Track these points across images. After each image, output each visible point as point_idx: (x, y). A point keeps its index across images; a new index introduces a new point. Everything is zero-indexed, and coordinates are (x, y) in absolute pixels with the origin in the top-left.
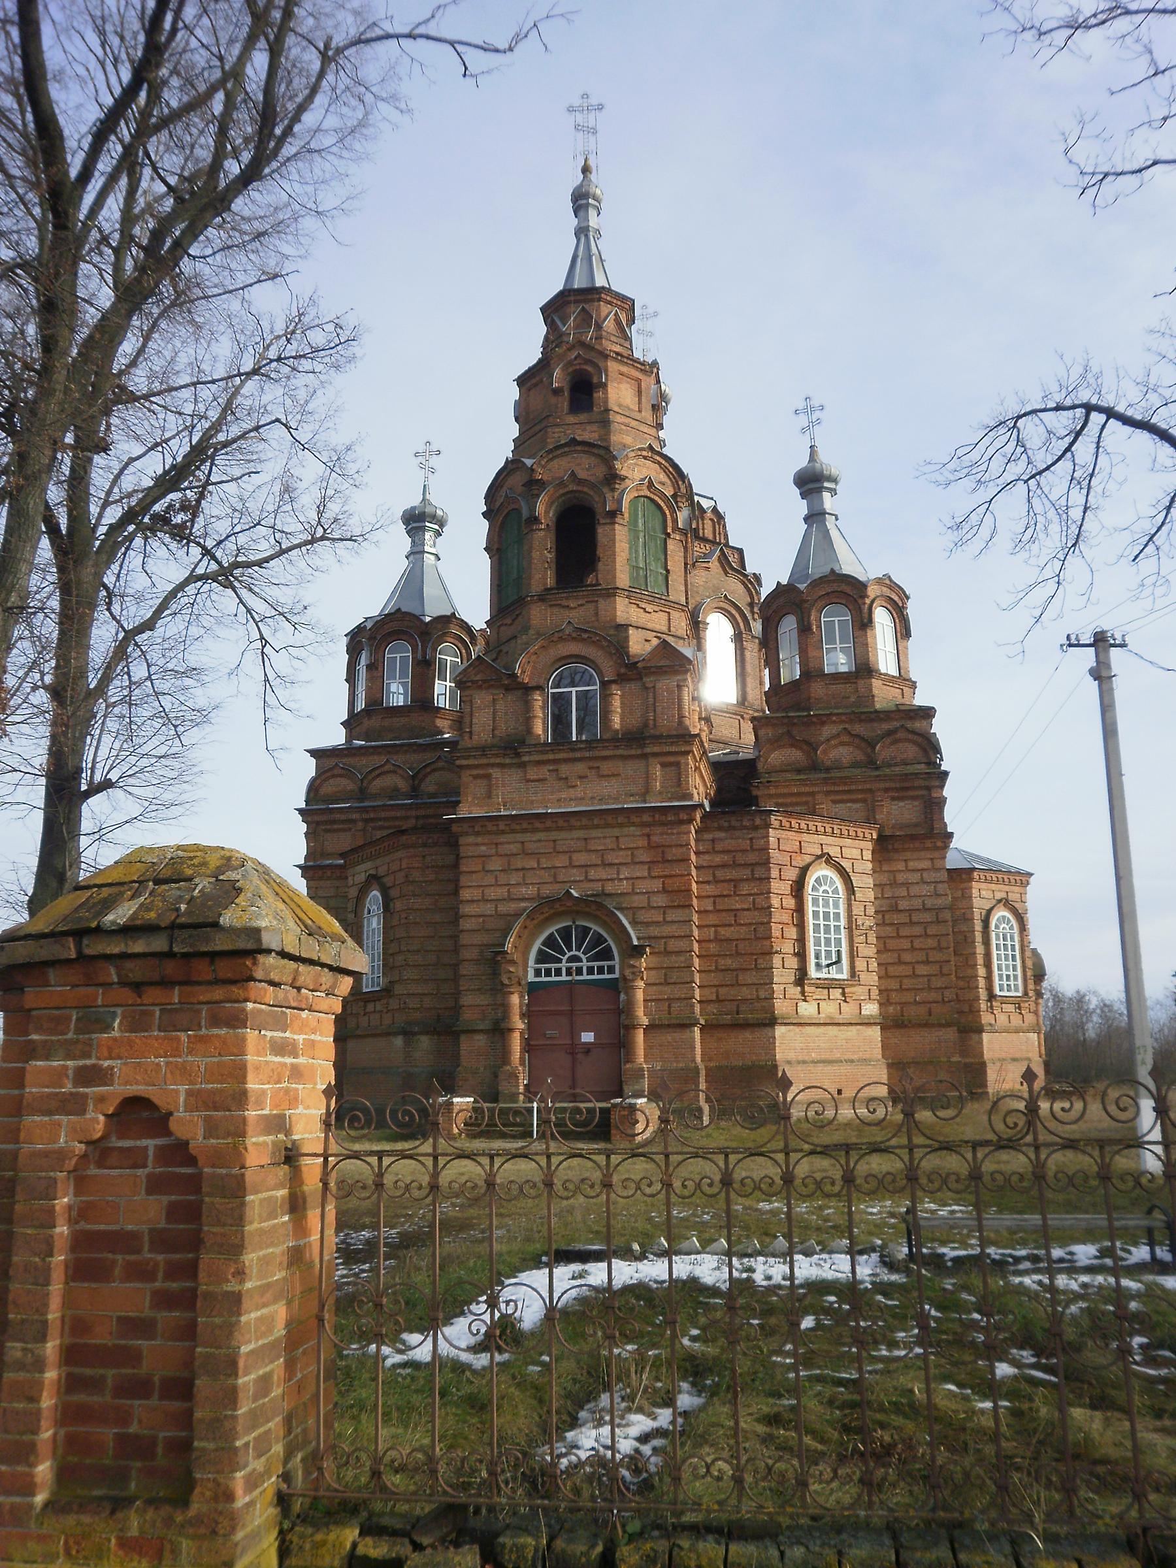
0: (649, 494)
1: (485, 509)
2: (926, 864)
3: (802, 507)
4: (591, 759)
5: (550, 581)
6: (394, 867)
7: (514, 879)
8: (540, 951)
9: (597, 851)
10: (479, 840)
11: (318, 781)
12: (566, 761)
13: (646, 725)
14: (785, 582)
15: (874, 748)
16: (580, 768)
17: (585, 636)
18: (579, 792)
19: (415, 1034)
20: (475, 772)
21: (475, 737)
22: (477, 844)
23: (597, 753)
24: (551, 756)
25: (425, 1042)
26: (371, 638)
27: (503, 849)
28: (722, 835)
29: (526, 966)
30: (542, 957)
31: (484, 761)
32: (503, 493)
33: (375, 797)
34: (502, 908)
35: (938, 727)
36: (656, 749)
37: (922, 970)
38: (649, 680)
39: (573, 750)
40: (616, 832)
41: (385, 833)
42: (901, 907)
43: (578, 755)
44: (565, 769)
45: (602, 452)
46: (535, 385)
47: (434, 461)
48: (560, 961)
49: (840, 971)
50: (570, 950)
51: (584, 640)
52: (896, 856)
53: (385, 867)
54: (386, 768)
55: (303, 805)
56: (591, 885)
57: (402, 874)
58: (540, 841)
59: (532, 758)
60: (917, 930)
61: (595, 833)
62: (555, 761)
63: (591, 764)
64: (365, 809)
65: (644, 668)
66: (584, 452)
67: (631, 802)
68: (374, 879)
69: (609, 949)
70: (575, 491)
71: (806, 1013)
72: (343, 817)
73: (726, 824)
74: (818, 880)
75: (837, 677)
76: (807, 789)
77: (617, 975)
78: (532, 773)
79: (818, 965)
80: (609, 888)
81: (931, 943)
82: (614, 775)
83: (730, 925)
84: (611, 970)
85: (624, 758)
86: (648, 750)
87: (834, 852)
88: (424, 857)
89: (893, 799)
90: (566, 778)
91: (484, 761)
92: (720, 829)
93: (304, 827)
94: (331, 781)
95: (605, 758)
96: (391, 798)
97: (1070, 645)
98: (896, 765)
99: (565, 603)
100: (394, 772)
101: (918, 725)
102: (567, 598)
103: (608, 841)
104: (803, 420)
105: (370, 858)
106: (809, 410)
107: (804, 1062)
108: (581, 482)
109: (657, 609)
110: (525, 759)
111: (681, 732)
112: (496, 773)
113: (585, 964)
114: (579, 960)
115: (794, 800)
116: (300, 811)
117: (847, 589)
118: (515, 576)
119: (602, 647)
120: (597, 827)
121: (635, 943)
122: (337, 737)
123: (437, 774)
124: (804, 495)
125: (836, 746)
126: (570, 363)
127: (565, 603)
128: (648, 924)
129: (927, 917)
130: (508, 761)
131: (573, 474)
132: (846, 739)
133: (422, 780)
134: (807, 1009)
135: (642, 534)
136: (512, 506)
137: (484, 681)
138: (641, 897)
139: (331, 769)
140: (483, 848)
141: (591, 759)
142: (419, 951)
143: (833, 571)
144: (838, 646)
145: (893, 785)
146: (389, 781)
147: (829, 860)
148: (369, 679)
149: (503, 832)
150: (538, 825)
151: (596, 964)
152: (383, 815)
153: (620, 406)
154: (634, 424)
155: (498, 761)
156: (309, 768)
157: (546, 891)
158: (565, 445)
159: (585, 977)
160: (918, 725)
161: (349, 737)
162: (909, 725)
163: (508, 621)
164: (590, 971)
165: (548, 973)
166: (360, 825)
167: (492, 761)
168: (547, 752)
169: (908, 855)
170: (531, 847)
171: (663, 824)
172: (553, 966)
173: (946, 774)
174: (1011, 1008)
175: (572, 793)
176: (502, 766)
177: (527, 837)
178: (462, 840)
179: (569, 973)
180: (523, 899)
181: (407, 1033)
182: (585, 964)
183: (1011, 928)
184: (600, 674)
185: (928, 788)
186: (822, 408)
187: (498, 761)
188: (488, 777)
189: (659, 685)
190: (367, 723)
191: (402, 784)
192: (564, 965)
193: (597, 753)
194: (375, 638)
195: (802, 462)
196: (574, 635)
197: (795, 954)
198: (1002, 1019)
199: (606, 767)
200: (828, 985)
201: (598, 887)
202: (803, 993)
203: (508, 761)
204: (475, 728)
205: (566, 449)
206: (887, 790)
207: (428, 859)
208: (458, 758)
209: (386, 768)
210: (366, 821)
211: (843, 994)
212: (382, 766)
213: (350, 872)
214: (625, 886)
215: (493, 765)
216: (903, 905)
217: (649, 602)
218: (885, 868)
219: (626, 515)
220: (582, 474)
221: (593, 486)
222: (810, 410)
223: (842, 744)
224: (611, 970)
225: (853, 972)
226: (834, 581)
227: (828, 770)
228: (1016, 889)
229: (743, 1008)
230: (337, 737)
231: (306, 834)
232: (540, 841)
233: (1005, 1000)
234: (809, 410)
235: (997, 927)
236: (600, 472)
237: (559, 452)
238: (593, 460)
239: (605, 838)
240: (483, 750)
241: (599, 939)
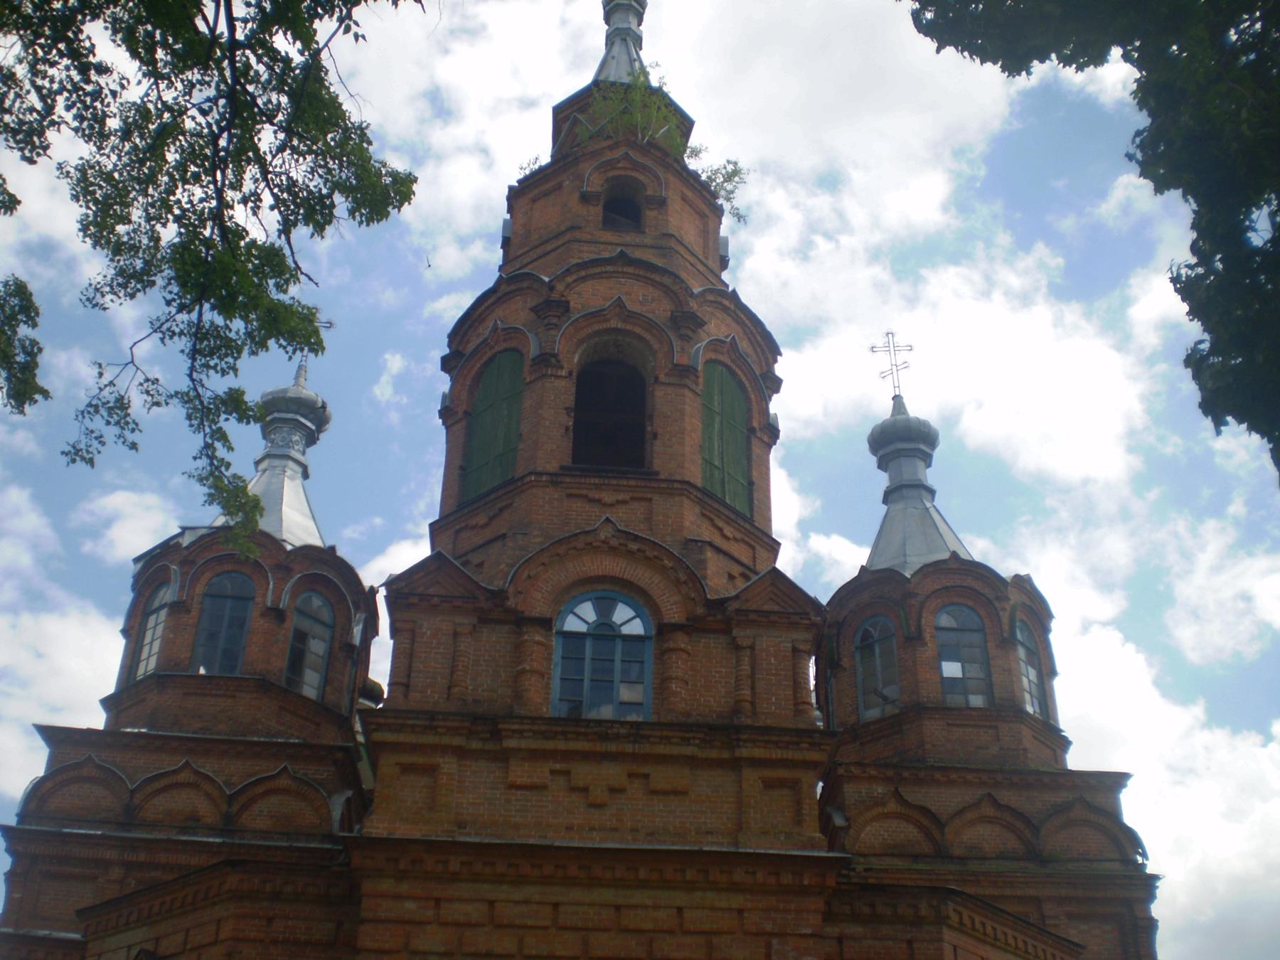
0: (729, 363)
4: (635, 757)
9: (639, 931)
10: (404, 888)
11: (49, 785)
12: (586, 756)
13: (736, 711)
16: (614, 773)
17: (634, 546)
20: (407, 759)
22: (398, 897)
23: (646, 748)
24: (561, 745)
28: (858, 930)
31: (430, 739)
32: (485, 330)
36: (758, 753)
38: (743, 635)
40: (680, 898)
43: (613, 747)
44: (583, 773)
45: (667, 280)
46: (546, 194)
51: (631, 553)
58: (526, 902)
59: (524, 744)
62: (567, 755)
64: (133, 845)
65: (738, 611)
66: (637, 277)
67: (713, 843)
70: (616, 330)
73: (867, 910)
78: (521, 772)
82: (676, 793)
85: (693, 762)
86: (744, 752)
88: (270, 920)
89: (1070, 916)
90: (585, 790)
91: (430, 739)
96: (183, 830)
99: (594, 494)
100: (194, 786)
102: (598, 487)
104: (883, 361)
108: (631, 316)
109: (739, 536)
110: (511, 743)
111: (802, 726)
112: (448, 765)
116: (7, 831)
117: (977, 585)
120: (643, 885)
122: (97, 720)
124: (882, 465)
126: (610, 164)
127: (594, 494)
130: (475, 745)
131: (619, 303)
132: (989, 811)
133: (246, 807)
135: (717, 419)
136: (513, 344)
140: (410, 905)
141: (635, 757)
146: (182, 801)
149: (455, 878)
154: (701, 268)
155: (457, 741)
163: (482, 519)
166: (116, 873)
167: (446, 740)
173: (1155, 878)
176: (462, 753)
178: (367, 886)
187: (457, 741)
188: (432, 770)
191: (205, 809)
193: (646, 748)
194: (193, 562)
196: (614, 542)
199: (662, 776)
203: (475, 745)
205: (609, 268)
212: (174, 772)
215: (445, 750)
217: (729, 521)
219: (701, 380)
221: (650, 325)
227: (962, 860)
230: (97, 720)
232: (526, 902)
237: (598, 270)
239: (656, 907)
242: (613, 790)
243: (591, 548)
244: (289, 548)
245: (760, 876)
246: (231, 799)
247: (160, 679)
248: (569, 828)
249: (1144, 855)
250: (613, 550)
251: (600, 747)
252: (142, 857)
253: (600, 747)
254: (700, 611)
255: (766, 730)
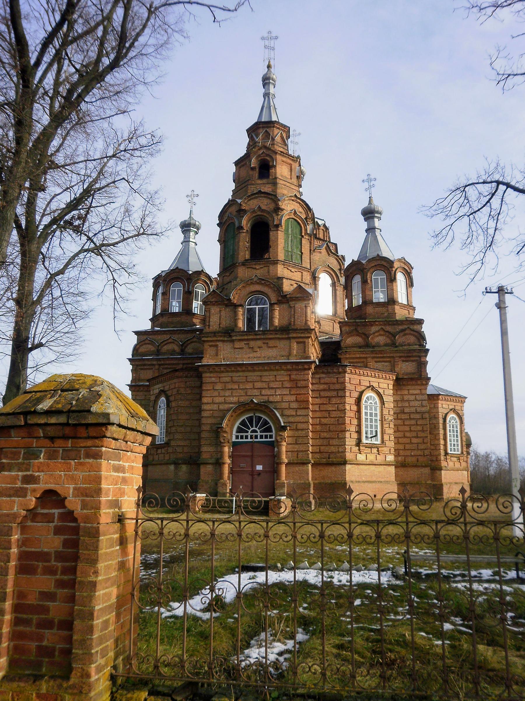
1: (218, 222)
2: (418, 392)
3: (365, 225)
4: (264, 339)
5: (248, 257)
6: (172, 387)
7: (227, 393)
8: (238, 427)
10: (212, 375)
12: (253, 339)
13: (290, 324)
14: (356, 259)
15: (395, 337)
16: (259, 343)
17: (263, 282)
18: (258, 354)
19: (179, 464)
20: (211, 344)
21: (211, 328)
22: (211, 377)
23: (267, 336)
24: (246, 337)
25: (184, 468)
26: (164, 281)
27: (222, 380)
28: (324, 376)
29: (232, 434)
30: (239, 430)
33: (164, 354)
34: (221, 407)
35: (425, 328)
36: (294, 335)
37: (414, 440)
38: (292, 303)
39: (256, 335)
40: (275, 373)
41: (168, 371)
42: (405, 411)
43: (258, 337)
44: (252, 343)
45: (273, 197)
46: (243, 165)
47: (195, 199)
48: (247, 432)
49: (377, 440)
50: (252, 427)
52: (404, 388)
53: (168, 387)
54: (170, 341)
55: (131, 357)
56: (263, 397)
57: (176, 390)
60: (413, 422)
61: (265, 373)
62: (248, 340)
63: (264, 341)
64: (159, 360)
66: (265, 197)
68: (162, 392)
69: (270, 427)
71: (361, 459)
72: (149, 363)
74: (367, 398)
75: (379, 304)
76: (364, 356)
77: (273, 439)
78: (237, 345)
79: (367, 437)
80: (271, 399)
81: (419, 428)
82: (274, 347)
83: (326, 418)
84: (271, 437)
86: (291, 336)
87: (375, 385)
89: (403, 361)
92: (323, 373)
93: (131, 367)
94: (144, 346)
95: (271, 339)
96: (172, 355)
97: (487, 292)
98: (405, 345)
99: (254, 266)
101: (416, 327)
102: (255, 264)
103: (271, 377)
104: (366, 185)
105: (161, 382)
106: (369, 180)
107: (359, 482)
108: (263, 211)
110: (234, 338)
111: (306, 328)
112: (220, 344)
113: (259, 434)
114: (256, 432)
115: (357, 360)
118: (231, 253)
119: (271, 288)
120: (266, 370)
121: (283, 424)
122: (147, 326)
123: (193, 344)
124: (366, 220)
125: (377, 336)
127: (254, 266)
128: (288, 416)
129: (418, 416)
130: (226, 339)
131: (259, 207)
132: (382, 333)
133: (186, 347)
134: (361, 457)
137: (216, 302)
138: (286, 404)
139: (144, 341)
140: (213, 379)
141: (264, 339)
142: (182, 426)
143: (378, 255)
144: (380, 290)
145: (403, 355)
146: (170, 347)
147: (373, 389)
148: (163, 299)
149: (223, 372)
150: (239, 369)
151: (264, 434)
152: (167, 362)
153: (282, 176)
154: (288, 184)
155: (221, 339)
156: (134, 340)
157: (242, 399)
158: (256, 193)
159: (259, 440)
160: (416, 327)
161: (153, 326)
162: (412, 327)
163: (228, 274)
164: (261, 437)
165: (242, 437)
166: (157, 367)
167: (219, 339)
168: (244, 335)
169: (409, 387)
170: (235, 379)
171: (297, 370)
172: (244, 434)
173: (428, 350)
174: (455, 459)
175: (255, 354)
176: (223, 341)
177: (234, 374)
178: (204, 375)
179: (251, 438)
180: (231, 403)
181: (176, 464)
182: (259, 434)
183: (456, 422)
184: (269, 300)
185: (420, 357)
186: (375, 179)
187: (221, 339)
188: (216, 346)
189: (297, 306)
190: (161, 320)
191: (177, 348)
192: (249, 434)
193: (267, 336)
195: (366, 204)
197: (356, 432)
198: (451, 464)
199: (271, 343)
200: (371, 446)
201: (266, 398)
202: (359, 450)
203: (226, 339)
204: (211, 323)
206: (400, 357)
207: (188, 383)
208: (203, 337)
209: (170, 341)
210: (160, 365)
211: (378, 451)
213: (152, 388)
214: (278, 398)
215: (219, 341)
216: (407, 410)
217: (293, 267)
218: (399, 393)
220: (263, 207)
221: (268, 213)
222: (369, 180)
223: (381, 335)
224: (271, 437)
225: (383, 441)
226: (378, 260)
227: (373, 347)
228: (459, 404)
229: (331, 456)
230: (147, 326)
231: (132, 370)
233: (452, 456)
234: (369, 180)
235: (450, 422)
236: (272, 206)
238: (269, 201)
240: (214, 333)
241: (266, 423)
242: (259, 347)
243: (252, 283)
244: (191, 272)
245: (294, 366)
246: (182, 345)
247: (161, 314)
248: (249, 358)
249: (426, 343)
250: (258, 283)
251: (255, 337)
252: (162, 362)
253: (255, 337)
254: (280, 298)
255: (297, 329)
